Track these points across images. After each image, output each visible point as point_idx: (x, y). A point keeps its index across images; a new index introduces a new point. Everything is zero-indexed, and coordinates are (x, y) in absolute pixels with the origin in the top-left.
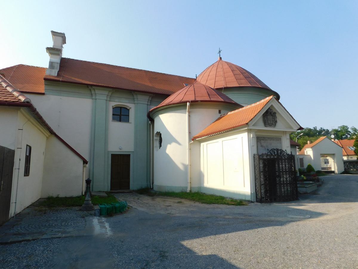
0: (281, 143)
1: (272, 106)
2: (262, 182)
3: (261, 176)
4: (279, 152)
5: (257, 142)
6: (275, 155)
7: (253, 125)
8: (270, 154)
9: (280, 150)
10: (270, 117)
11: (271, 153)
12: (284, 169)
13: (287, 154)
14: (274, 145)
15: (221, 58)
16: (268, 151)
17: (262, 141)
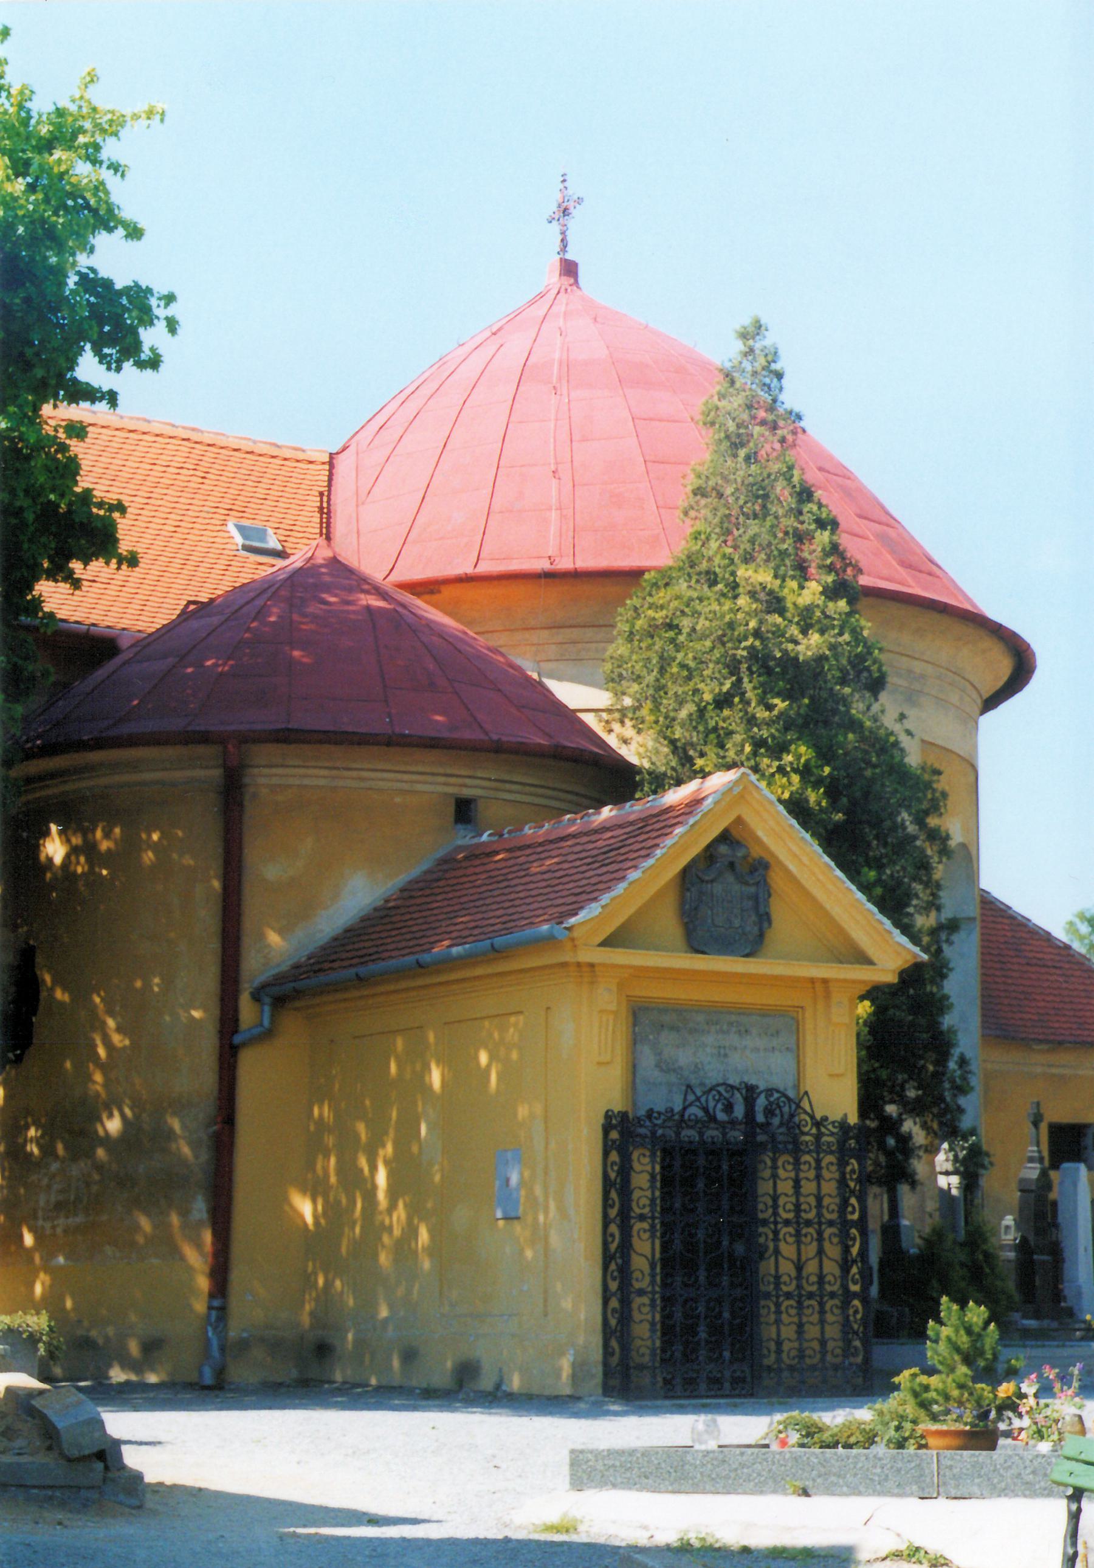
0: (797, 1051)
1: (739, 820)
2: (829, 1278)
3: (827, 1245)
4: (761, 1102)
5: (635, 1041)
6: (733, 1123)
7: (604, 944)
8: (700, 1114)
9: (769, 1091)
10: (726, 887)
11: (705, 1110)
12: (789, 1206)
13: (812, 1117)
14: (755, 1062)
15: (569, 269)
16: (691, 1098)
17: (667, 1038)
